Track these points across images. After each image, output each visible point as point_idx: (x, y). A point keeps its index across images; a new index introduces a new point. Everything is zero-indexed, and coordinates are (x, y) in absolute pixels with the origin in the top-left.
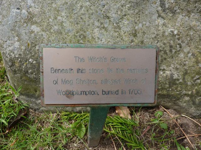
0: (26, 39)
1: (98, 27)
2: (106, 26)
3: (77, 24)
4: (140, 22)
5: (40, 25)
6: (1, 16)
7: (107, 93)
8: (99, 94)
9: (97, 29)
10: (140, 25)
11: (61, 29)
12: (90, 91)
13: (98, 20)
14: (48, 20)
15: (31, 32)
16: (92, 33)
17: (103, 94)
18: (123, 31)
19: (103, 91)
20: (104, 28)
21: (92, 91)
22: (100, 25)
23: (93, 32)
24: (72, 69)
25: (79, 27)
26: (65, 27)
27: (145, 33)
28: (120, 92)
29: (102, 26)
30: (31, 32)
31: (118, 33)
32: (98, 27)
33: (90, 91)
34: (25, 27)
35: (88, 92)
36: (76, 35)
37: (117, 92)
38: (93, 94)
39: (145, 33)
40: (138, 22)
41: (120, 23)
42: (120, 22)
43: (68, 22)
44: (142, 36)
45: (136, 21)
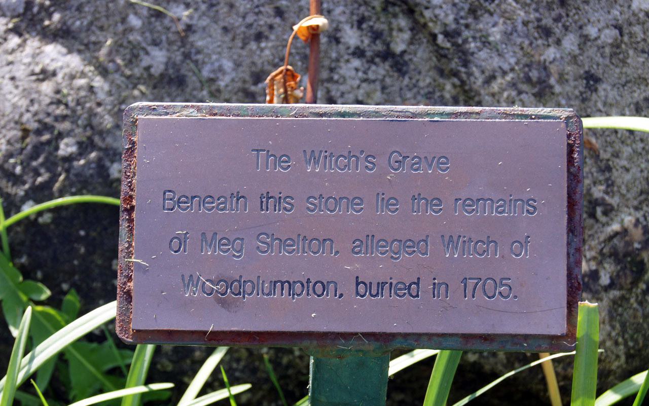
0: (15, 106)
1: (359, 53)
2: (399, 47)
3: (259, 37)
4: (566, 28)
5: (86, 41)
6: (47, 3)
7: (374, 292)
8: (341, 295)
9: (356, 63)
10: (570, 42)
11: (183, 62)
12: (308, 281)
13: (361, 22)
14: (124, 20)
15: (41, 77)
16: (330, 80)
17: (358, 294)
18: (483, 72)
19: (358, 284)
20: (387, 55)
21: (316, 283)
22: (367, 41)
23: (336, 77)
24: (243, 197)
25: (267, 52)
26: (198, 52)
27: (597, 80)
28: (426, 286)
29: (379, 47)
30: (41, 77)
31: (456, 81)
32: (359, 53)
33: (308, 281)
34: (13, 51)
35: (303, 285)
36: (253, 88)
37: (411, 288)
38: (319, 291)
39: (597, 80)
40: (558, 30)
41: (466, 33)
42: (467, 26)
43: (216, 31)
44: (581, 93)
45: (547, 21)
